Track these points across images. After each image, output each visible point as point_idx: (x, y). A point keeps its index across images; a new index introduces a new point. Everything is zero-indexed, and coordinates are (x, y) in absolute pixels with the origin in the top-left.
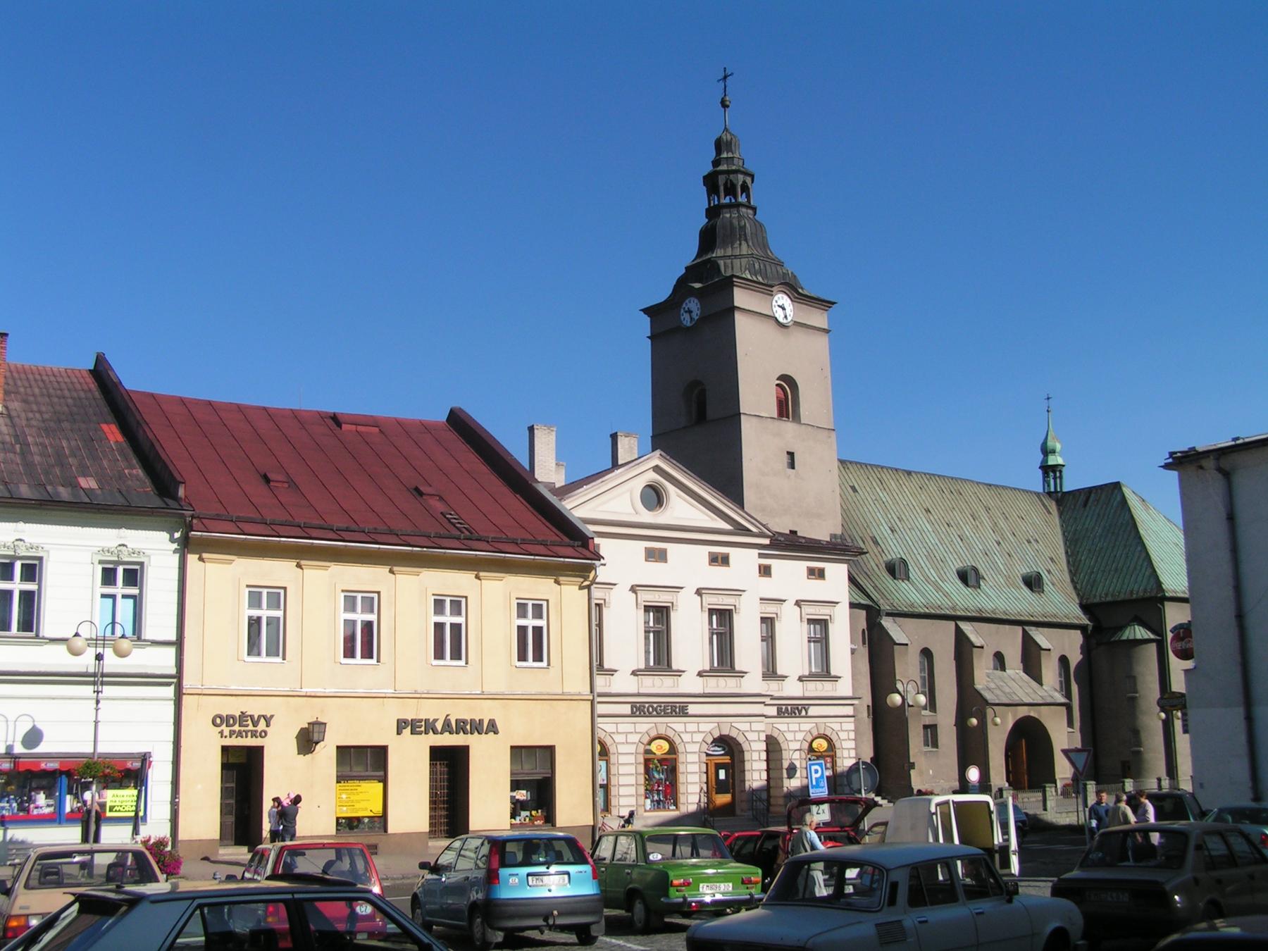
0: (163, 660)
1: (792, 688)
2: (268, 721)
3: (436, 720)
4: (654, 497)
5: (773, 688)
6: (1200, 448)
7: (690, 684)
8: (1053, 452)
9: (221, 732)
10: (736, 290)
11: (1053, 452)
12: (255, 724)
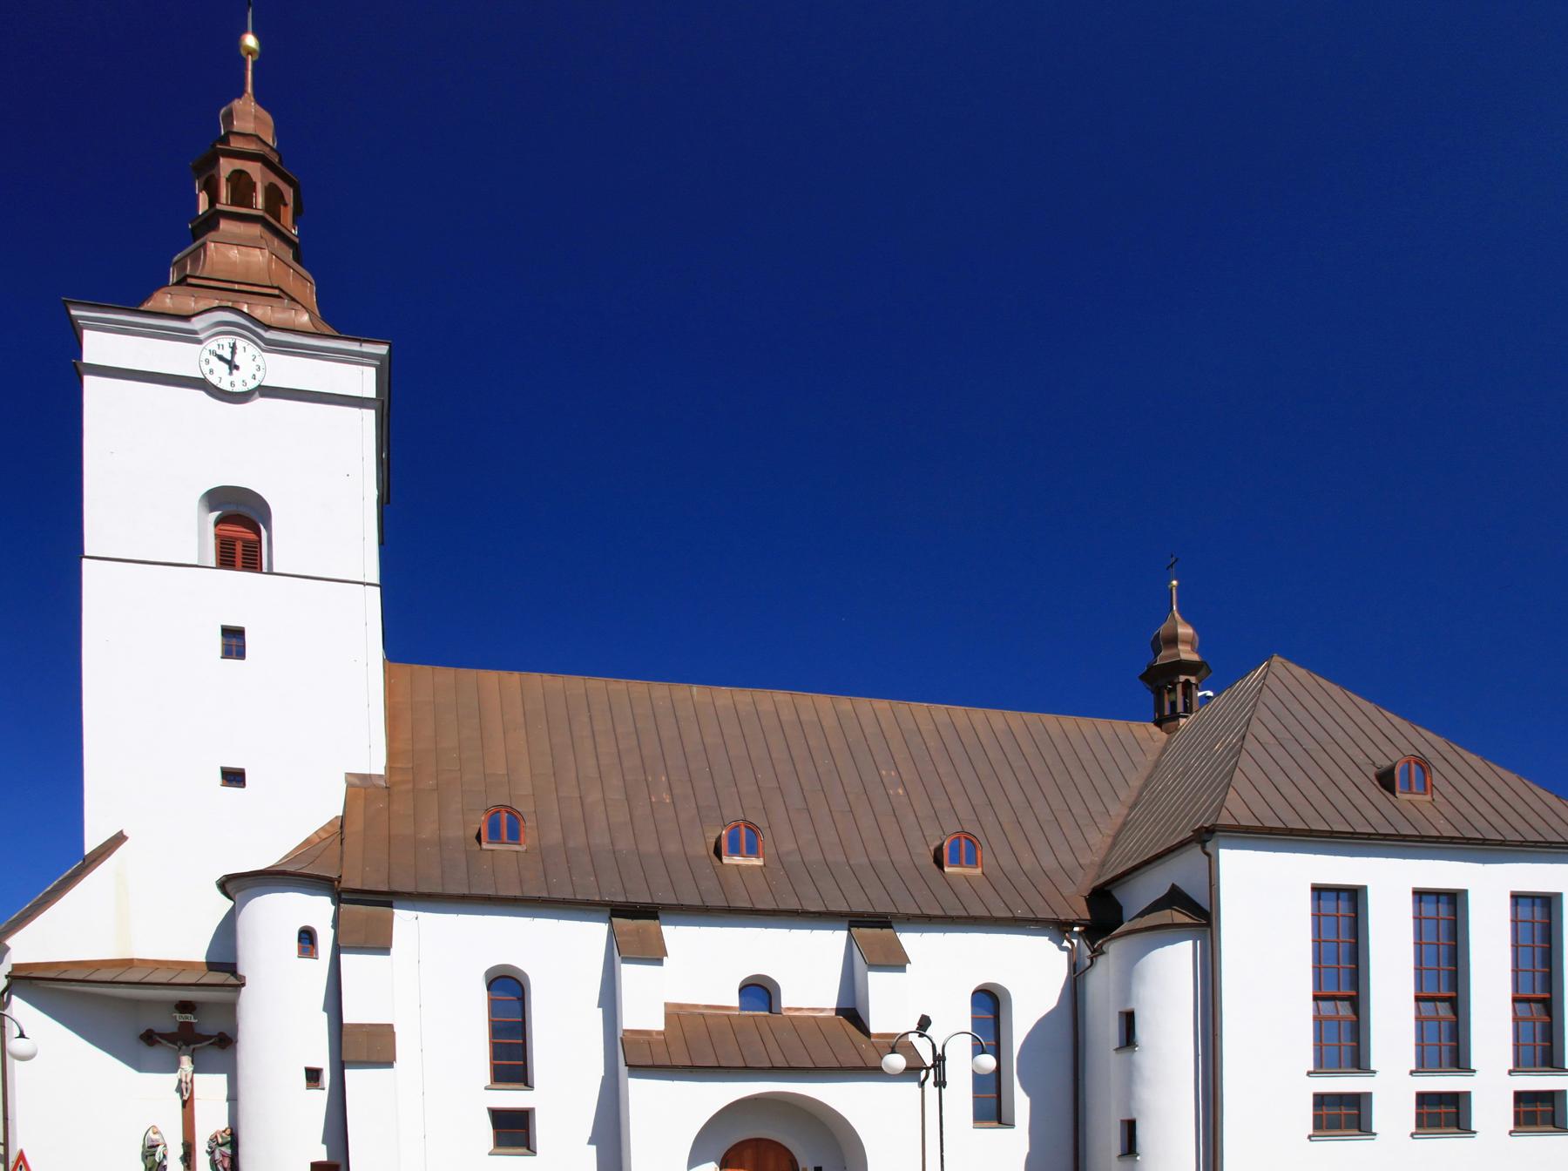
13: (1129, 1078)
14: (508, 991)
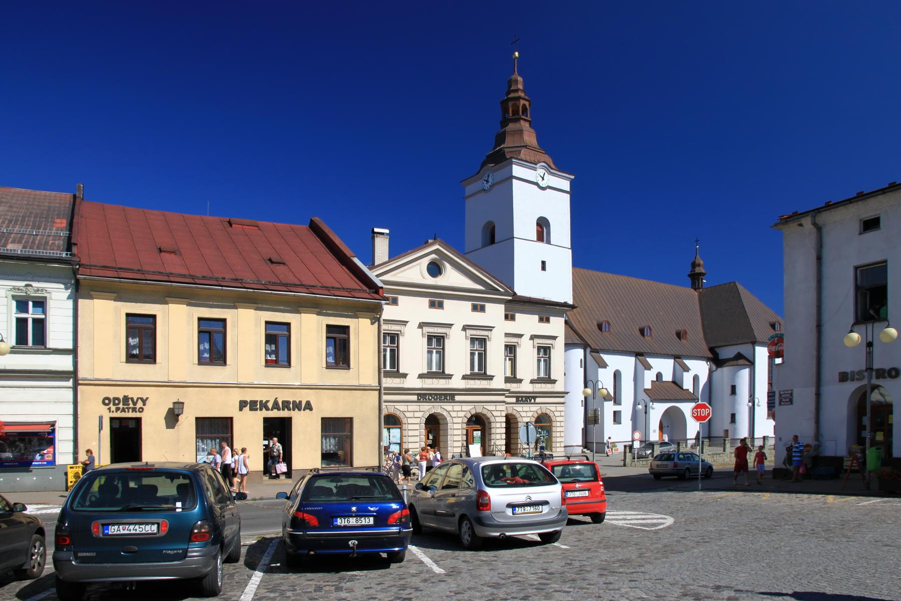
0: (64, 363)
1: (526, 387)
2: (144, 401)
3: (267, 401)
4: (435, 269)
5: (514, 387)
6: (582, 426)
7: (457, 383)
8: (699, 265)
9: (109, 409)
10: (514, 166)
11: (699, 265)
12: (135, 403)
13: (733, 404)
14: (617, 376)
